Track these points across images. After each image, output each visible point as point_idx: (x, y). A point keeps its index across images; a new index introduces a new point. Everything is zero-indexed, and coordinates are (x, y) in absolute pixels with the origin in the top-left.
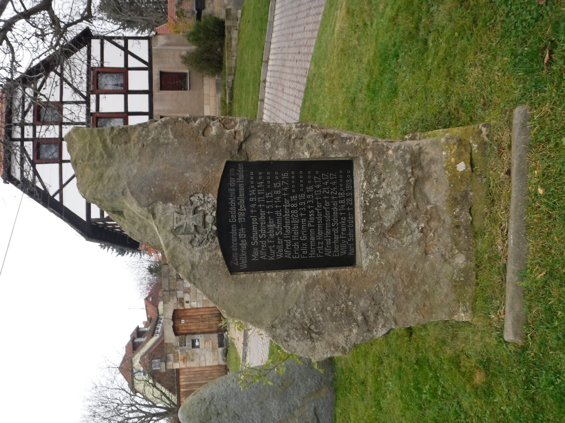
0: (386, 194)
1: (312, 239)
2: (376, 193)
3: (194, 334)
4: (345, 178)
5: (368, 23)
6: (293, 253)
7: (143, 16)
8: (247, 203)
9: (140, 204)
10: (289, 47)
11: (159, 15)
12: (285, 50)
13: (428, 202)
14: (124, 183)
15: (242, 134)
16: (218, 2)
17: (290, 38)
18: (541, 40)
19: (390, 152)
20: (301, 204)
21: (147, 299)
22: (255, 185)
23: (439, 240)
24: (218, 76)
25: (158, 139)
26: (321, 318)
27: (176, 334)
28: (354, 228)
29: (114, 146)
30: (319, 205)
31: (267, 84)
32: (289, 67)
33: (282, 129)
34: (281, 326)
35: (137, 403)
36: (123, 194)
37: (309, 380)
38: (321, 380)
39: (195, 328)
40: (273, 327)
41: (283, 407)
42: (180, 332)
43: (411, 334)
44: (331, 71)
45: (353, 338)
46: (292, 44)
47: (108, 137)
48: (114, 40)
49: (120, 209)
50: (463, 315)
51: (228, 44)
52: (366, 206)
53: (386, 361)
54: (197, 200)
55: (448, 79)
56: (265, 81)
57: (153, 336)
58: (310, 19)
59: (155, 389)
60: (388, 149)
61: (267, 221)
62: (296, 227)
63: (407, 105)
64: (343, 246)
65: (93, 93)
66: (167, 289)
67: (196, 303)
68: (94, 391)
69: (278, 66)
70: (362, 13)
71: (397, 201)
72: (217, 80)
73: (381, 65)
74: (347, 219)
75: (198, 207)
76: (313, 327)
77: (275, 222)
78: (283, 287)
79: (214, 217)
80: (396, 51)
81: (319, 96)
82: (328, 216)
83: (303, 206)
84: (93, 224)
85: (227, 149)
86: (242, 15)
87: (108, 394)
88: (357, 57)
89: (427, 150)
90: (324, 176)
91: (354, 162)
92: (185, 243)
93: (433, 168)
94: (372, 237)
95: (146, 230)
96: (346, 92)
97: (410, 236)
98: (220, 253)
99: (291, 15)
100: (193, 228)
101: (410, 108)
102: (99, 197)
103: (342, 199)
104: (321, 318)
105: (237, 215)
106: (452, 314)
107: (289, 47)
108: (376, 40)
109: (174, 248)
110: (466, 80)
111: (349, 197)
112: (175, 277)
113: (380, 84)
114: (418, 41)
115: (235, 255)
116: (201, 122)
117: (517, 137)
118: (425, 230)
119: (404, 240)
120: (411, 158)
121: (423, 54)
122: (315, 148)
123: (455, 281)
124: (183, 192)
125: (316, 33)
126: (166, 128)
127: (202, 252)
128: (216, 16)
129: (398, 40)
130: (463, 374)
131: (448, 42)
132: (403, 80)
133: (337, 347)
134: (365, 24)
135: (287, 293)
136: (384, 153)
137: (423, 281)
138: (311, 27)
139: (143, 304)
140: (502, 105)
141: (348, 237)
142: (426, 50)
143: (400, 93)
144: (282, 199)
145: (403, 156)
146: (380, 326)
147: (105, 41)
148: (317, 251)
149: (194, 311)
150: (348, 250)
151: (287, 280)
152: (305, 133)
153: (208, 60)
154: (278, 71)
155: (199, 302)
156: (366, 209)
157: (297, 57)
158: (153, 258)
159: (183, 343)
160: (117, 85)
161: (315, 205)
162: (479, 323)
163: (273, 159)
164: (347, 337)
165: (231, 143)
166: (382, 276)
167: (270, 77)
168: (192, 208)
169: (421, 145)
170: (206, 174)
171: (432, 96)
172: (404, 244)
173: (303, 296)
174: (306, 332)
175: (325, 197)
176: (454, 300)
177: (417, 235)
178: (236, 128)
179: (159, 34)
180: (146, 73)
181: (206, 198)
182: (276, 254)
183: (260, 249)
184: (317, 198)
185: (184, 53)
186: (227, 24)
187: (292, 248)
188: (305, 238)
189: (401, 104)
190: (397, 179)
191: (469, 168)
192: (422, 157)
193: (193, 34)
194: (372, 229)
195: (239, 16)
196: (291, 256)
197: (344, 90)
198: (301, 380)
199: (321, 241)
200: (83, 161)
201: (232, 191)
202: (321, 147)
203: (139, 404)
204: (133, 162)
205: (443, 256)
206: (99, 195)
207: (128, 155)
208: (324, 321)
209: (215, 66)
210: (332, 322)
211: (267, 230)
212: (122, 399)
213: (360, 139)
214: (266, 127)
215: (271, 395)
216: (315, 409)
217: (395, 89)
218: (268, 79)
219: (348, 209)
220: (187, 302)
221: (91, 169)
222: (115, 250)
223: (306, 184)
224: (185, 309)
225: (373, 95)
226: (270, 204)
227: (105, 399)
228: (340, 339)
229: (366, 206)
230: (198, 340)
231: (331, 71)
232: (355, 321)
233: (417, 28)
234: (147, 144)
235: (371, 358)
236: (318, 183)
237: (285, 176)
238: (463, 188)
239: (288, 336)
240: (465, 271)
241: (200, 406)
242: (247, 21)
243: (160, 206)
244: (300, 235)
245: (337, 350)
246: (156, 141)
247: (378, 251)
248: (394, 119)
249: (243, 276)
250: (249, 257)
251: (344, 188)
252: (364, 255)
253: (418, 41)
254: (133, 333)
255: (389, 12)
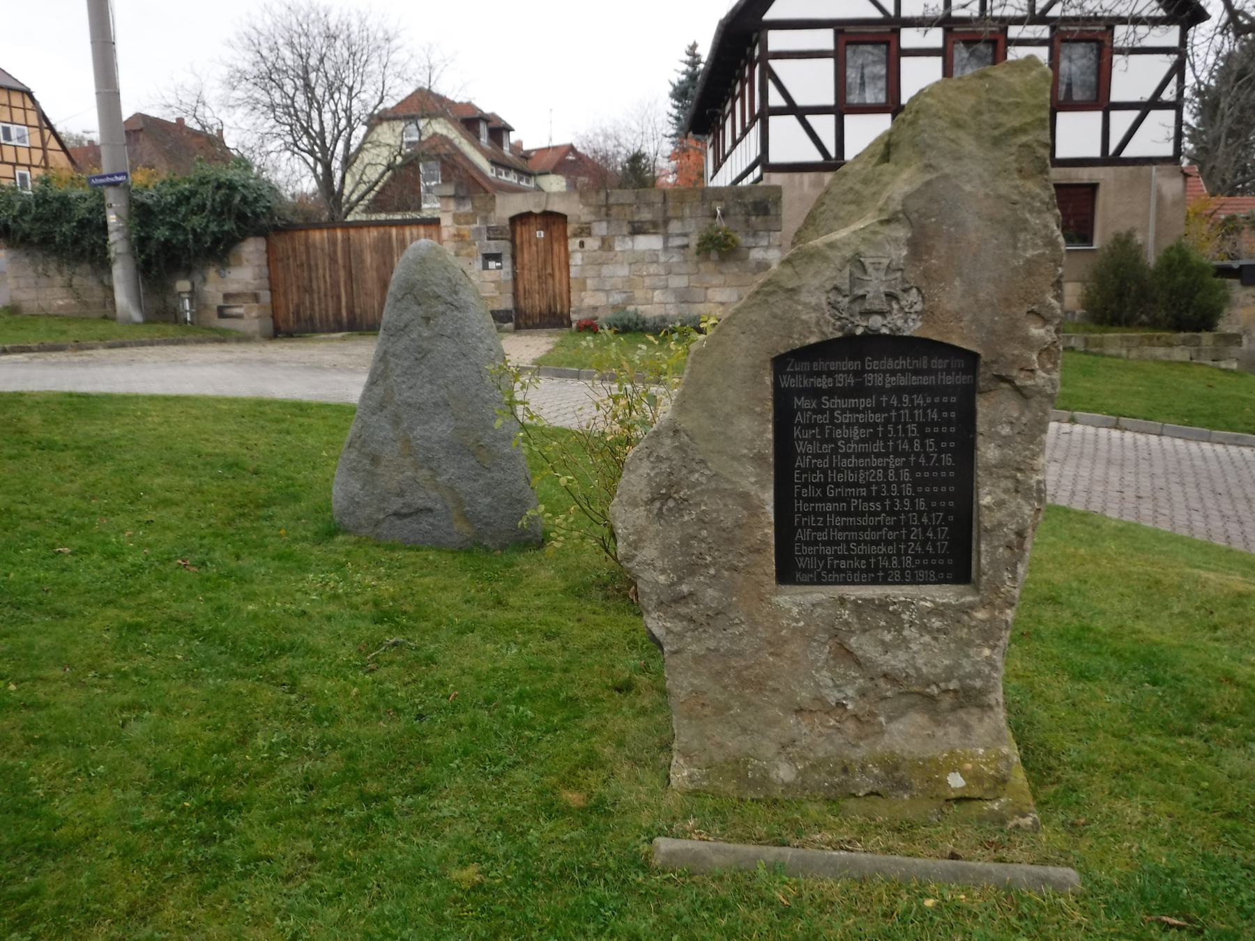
0: (909, 642)
1: (829, 507)
2: (912, 624)
3: (514, 258)
4: (938, 569)
5: (1219, 633)
6: (804, 471)
7: (1228, 137)
8: (899, 391)
9: (908, 197)
10: (1152, 476)
11: (1228, 176)
12: (1144, 466)
13: (890, 719)
14: (947, 167)
15: (1029, 383)
16: (1247, 309)
17: (1173, 478)
18: (1203, 913)
19: (987, 652)
20: (894, 487)
21: (571, 148)
22: (932, 406)
23: (821, 735)
24: (1084, 316)
25: (1025, 229)
26: (686, 518)
27: (514, 220)
28: (845, 583)
29: (1014, 149)
30: (891, 520)
31: (1066, 427)
32: (1107, 474)
33: (1034, 456)
34: (676, 447)
35: (353, 129)
36: (928, 167)
37: (489, 500)
38: (487, 524)
39: (526, 261)
40: (676, 432)
41: (436, 446)
42: (518, 229)
43: (619, 690)
44: (1111, 559)
45: (648, 575)
46: (1160, 482)
47: (1030, 137)
48: (1175, 79)
49: (893, 157)
50: (685, 774)
51: (1159, 338)
52: (888, 604)
53: (554, 645)
54: (910, 299)
55: (1116, 768)
56: (1073, 421)
57: (493, 163)
58: (1216, 523)
59: (381, 169)
60: (993, 648)
61: (865, 426)
62: (851, 478)
63: (1059, 696)
64: (812, 563)
65: (1053, 29)
66: (612, 200)
67: (580, 262)
68: (380, 35)
69: (1109, 451)
70: (1239, 623)
71: (896, 661)
72: (1074, 313)
73: (1133, 653)
74: (862, 571)
75: (898, 303)
76: (671, 504)
77: (862, 441)
78: (745, 451)
79: (878, 330)
80: (1164, 681)
81: (1053, 535)
82: (869, 535)
83: (889, 490)
84: (755, 36)
85: (1003, 356)
86: (1225, 370)
87: (374, 66)
88: (1145, 610)
89: (987, 720)
90: (942, 531)
91: (967, 587)
92: (834, 278)
93: (954, 731)
94: (830, 615)
95: (852, 202)
96: (1071, 589)
97: (830, 683)
98: (813, 340)
99: (1226, 481)
100: (861, 292)
101: (1052, 702)
102: (921, 122)
103: (900, 563)
104: (686, 518)
105: (878, 371)
106: (686, 754)
107: (1152, 476)
108: (1186, 647)
109: (826, 259)
110: (1117, 797)
111: (903, 576)
112: (636, 218)
113: (1094, 650)
114: (1187, 719)
115: (805, 366)
116: (1053, 308)
117: (1021, 870)
118: (840, 711)
119: (824, 673)
120: (975, 688)
121: (1161, 727)
122: (998, 515)
123: (746, 763)
124: (926, 275)
125: (1185, 532)
126: (1045, 245)
127: (817, 308)
128: (1226, 311)
129: (1186, 684)
130: (572, 773)
131: (1189, 769)
132: (1107, 691)
133: (635, 545)
134: (1215, 628)
135: (734, 458)
136: (986, 640)
137: (747, 704)
138: (1199, 524)
139: (561, 140)
140: (1076, 852)
141: (829, 572)
142: (1171, 734)
143: (1080, 686)
144: (904, 454)
145: (979, 674)
146: (668, 625)
147: (1174, 57)
148: (805, 514)
149: (563, 259)
150: (806, 571)
151: (759, 459)
152: (1027, 496)
153: (1120, 295)
154: (1096, 449)
155: (583, 270)
156: (882, 606)
157: (1130, 493)
158: (663, 163)
159: (494, 234)
160: (1069, 86)
161: (891, 513)
162: (671, 801)
163: (980, 439)
164: (652, 564)
165: (1013, 362)
166: (760, 629)
167: (1083, 434)
168: (898, 292)
169: (996, 709)
170: (958, 316)
171: (1080, 740)
172: (817, 671)
173: (728, 486)
174: (663, 491)
175: (904, 532)
176: (711, 759)
177: (833, 697)
178: (1040, 373)
179: (1185, 181)
180: (1096, 152)
181: (914, 316)
182: (804, 440)
183: (815, 411)
184: (903, 517)
185: (1139, 238)
186: (1206, 337)
187: (813, 470)
188: (831, 494)
189: (1059, 688)
190: (936, 662)
191: (953, 795)
192: (974, 710)
193: (1185, 259)
194: (846, 614)
195: (1223, 365)
196: (799, 467)
197: (1075, 584)
198: (489, 484)
199: (825, 522)
200: (987, 91)
201: (923, 363)
202: (1000, 525)
203: (350, 134)
204: (984, 184)
205: (793, 742)
206: (926, 121)
207: (998, 174)
208: (683, 524)
209: (1106, 309)
210: (680, 539)
211: (849, 425)
212: (363, 96)
213: (1013, 597)
214: (1040, 426)
215: (460, 424)
216: (430, 510)
217: (1086, 677)
218: (1078, 428)
219: (881, 574)
220: (582, 244)
221: (973, 107)
222: (684, 77)
223: (929, 498)
224: (566, 239)
225: (1071, 638)
226: (896, 431)
227: (364, 58)
228: (649, 552)
229: (888, 604)
230: (499, 268)
231: (1111, 559)
232: (681, 580)
233: (1212, 719)
234: (1015, 210)
235: (553, 619)
236: (930, 519)
237: (947, 459)
238: (916, 783)
239: (659, 459)
240: (764, 781)
241: (444, 283)
242: (1211, 383)
243: (902, 233)
244: (837, 485)
245: (630, 545)
246: (1022, 225)
247: (807, 624)
248: (1028, 674)
249: (768, 380)
250: (800, 392)
251: (920, 567)
252: (798, 598)
253: (1187, 719)
254: (499, 119)
255: (1243, 672)
